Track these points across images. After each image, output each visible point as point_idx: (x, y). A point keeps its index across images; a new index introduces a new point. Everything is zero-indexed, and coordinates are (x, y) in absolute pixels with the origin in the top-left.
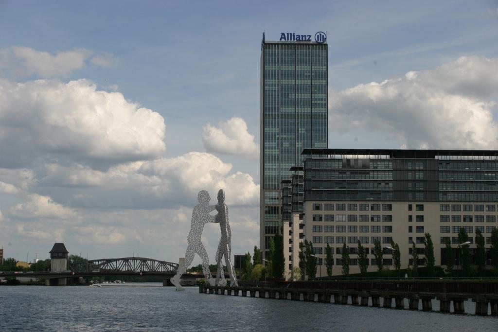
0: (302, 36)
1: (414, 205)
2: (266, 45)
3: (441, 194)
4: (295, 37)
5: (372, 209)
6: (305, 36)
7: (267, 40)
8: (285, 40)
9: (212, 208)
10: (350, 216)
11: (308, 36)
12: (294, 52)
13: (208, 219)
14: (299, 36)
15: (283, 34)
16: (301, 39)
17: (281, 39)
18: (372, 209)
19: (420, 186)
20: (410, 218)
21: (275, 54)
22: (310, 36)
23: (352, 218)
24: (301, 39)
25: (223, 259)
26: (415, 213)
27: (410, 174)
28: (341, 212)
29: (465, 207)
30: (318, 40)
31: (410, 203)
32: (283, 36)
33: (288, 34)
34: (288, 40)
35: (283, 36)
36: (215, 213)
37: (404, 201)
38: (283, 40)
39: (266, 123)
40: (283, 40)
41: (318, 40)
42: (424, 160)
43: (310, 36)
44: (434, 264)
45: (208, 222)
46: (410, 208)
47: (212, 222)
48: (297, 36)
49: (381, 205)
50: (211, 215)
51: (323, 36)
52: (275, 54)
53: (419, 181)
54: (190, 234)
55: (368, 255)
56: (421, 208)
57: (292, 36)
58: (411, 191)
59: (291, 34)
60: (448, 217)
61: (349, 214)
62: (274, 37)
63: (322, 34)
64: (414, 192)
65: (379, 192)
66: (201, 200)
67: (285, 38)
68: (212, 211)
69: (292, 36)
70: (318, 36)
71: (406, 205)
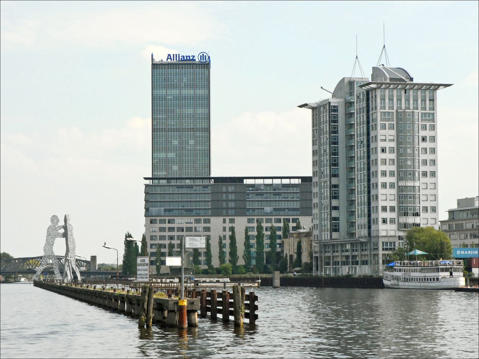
0: (187, 57)
1: (227, 219)
2: (155, 66)
3: (252, 210)
4: (180, 58)
5: (169, 222)
6: (189, 56)
7: (157, 60)
8: (171, 60)
9: (60, 228)
10: (204, 228)
11: (192, 56)
12: (179, 71)
13: (57, 235)
14: (184, 56)
15: (169, 55)
16: (185, 59)
17: (167, 60)
18: (169, 222)
19: (232, 205)
20: (224, 228)
21: (162, 73)
22: (194, 56)
23: (162, 229)
24: (185, 59)
25: (67, 263)
26: (228, 225)
27: (224, 195)
28: (180, 226)
29: (205, 220)
30: (201, 60)
31: (225, 218)
32: (169, 57)
33: (174, 55)
34: (174, 60)
35: (169, 57)
36: (62, 231)
37: (243, 216)
38: (169, 60)
39: (207, 105)
40: (169, 60)
41: (201, 60)
42: (226, 184)
43: (194, 56)
44: (236, 264)
45: (57, 237)
46: (224, 221)
47: (61, 237)
48: (181, 56)
49: (202, 220)
50: (60, 232)
51: (205, 56)
52: (162, 73)
53: (231, 201)
54: (45, 246)
55: (279, 272)
56: (232, 221)
57: (178, 57)
58: (225, 208)
59: (176, 55)
60: (165, 228)
61: (169, 227)
62: (161, 57)
63: (205, 54)
64: (227, 209)
65: (191, 210)
66: (53, 222)
67: (171, 58)
68: (60, 229)
69: (178, 57)
70: (201, 56)
71: (221, 219)
